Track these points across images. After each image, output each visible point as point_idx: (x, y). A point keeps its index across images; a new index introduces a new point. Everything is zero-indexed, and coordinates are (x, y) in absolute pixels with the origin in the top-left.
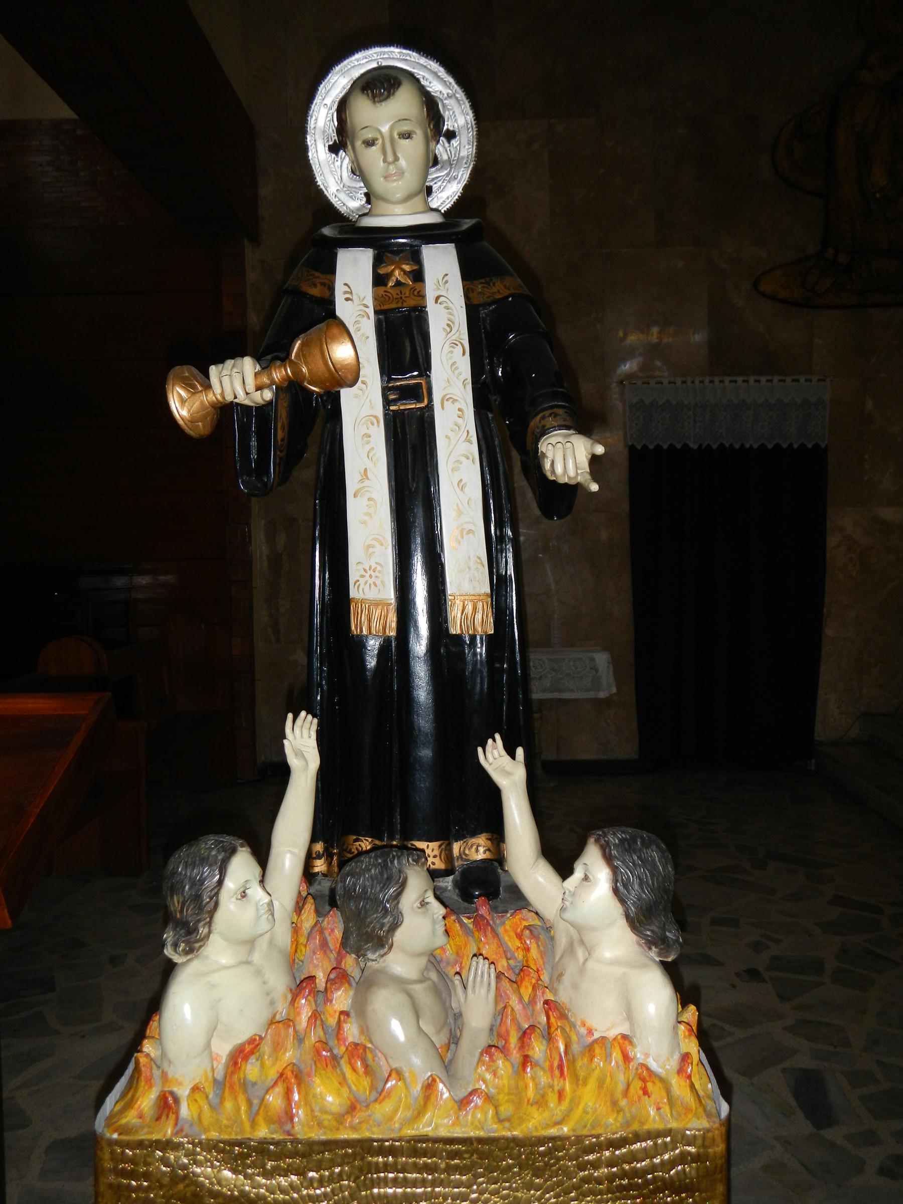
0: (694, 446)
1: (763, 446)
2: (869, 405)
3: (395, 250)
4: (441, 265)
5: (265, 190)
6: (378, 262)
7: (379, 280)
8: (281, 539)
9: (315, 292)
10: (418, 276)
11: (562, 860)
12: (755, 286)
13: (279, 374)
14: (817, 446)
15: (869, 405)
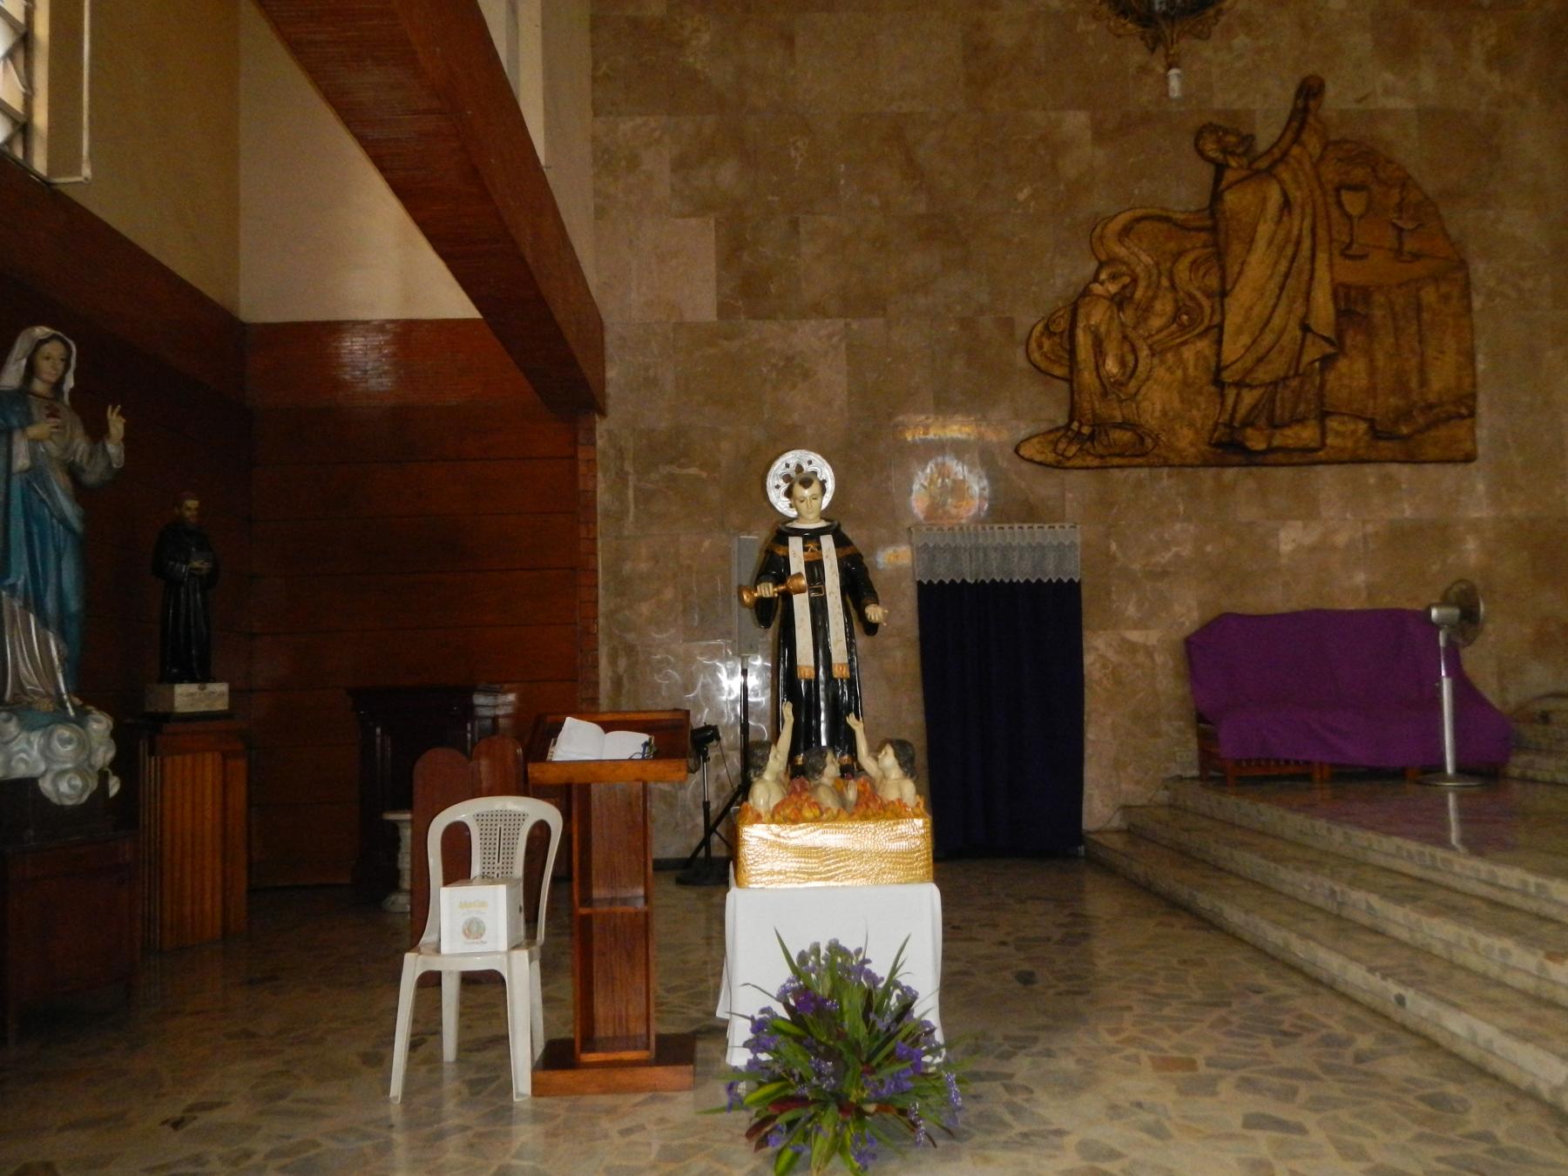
0: (970, 580)
1: (1027, 581)
2: (1114, 547)
3: (811, 537)
4: (827, 542)
5: (612, 373)
6: (804, 542)
7: (805, 549)
8: (622, 663)
9: (781, 553)
10: (820, 548)
11: (875, 751)
12: (1017, 451)
13: (782, 588)
14: (1071, 581)
15: (1114, 547)
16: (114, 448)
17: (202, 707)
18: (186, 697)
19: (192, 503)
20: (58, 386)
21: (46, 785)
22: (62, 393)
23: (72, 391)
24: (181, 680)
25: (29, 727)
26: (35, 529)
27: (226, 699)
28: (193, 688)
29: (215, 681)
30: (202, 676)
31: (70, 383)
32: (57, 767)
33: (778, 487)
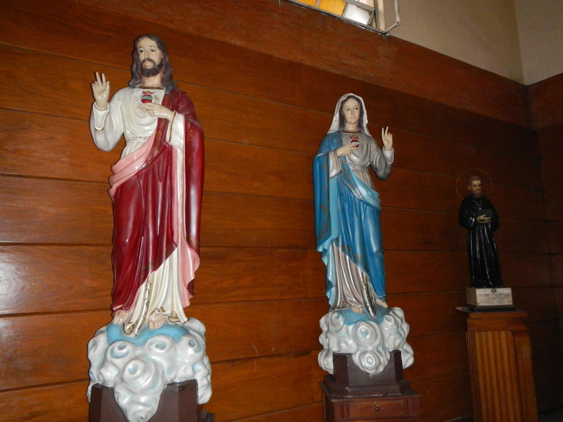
16: (389, 153)
17: (495, 303)
18: (483, 296)
19: (476, 182)
20: (360, 123)
21: (356, 359)
22: (362, 128)
23: (367, 125)
24: (481, 286)
25: (348, 322)
26: (346, 206)
27: (511, 298)
28: (488, 291)
29: (504, 286)
30: (495, 283)
31: (366, 121)
32: (362, 349)
33: (407, 352)
